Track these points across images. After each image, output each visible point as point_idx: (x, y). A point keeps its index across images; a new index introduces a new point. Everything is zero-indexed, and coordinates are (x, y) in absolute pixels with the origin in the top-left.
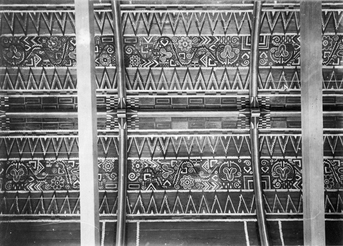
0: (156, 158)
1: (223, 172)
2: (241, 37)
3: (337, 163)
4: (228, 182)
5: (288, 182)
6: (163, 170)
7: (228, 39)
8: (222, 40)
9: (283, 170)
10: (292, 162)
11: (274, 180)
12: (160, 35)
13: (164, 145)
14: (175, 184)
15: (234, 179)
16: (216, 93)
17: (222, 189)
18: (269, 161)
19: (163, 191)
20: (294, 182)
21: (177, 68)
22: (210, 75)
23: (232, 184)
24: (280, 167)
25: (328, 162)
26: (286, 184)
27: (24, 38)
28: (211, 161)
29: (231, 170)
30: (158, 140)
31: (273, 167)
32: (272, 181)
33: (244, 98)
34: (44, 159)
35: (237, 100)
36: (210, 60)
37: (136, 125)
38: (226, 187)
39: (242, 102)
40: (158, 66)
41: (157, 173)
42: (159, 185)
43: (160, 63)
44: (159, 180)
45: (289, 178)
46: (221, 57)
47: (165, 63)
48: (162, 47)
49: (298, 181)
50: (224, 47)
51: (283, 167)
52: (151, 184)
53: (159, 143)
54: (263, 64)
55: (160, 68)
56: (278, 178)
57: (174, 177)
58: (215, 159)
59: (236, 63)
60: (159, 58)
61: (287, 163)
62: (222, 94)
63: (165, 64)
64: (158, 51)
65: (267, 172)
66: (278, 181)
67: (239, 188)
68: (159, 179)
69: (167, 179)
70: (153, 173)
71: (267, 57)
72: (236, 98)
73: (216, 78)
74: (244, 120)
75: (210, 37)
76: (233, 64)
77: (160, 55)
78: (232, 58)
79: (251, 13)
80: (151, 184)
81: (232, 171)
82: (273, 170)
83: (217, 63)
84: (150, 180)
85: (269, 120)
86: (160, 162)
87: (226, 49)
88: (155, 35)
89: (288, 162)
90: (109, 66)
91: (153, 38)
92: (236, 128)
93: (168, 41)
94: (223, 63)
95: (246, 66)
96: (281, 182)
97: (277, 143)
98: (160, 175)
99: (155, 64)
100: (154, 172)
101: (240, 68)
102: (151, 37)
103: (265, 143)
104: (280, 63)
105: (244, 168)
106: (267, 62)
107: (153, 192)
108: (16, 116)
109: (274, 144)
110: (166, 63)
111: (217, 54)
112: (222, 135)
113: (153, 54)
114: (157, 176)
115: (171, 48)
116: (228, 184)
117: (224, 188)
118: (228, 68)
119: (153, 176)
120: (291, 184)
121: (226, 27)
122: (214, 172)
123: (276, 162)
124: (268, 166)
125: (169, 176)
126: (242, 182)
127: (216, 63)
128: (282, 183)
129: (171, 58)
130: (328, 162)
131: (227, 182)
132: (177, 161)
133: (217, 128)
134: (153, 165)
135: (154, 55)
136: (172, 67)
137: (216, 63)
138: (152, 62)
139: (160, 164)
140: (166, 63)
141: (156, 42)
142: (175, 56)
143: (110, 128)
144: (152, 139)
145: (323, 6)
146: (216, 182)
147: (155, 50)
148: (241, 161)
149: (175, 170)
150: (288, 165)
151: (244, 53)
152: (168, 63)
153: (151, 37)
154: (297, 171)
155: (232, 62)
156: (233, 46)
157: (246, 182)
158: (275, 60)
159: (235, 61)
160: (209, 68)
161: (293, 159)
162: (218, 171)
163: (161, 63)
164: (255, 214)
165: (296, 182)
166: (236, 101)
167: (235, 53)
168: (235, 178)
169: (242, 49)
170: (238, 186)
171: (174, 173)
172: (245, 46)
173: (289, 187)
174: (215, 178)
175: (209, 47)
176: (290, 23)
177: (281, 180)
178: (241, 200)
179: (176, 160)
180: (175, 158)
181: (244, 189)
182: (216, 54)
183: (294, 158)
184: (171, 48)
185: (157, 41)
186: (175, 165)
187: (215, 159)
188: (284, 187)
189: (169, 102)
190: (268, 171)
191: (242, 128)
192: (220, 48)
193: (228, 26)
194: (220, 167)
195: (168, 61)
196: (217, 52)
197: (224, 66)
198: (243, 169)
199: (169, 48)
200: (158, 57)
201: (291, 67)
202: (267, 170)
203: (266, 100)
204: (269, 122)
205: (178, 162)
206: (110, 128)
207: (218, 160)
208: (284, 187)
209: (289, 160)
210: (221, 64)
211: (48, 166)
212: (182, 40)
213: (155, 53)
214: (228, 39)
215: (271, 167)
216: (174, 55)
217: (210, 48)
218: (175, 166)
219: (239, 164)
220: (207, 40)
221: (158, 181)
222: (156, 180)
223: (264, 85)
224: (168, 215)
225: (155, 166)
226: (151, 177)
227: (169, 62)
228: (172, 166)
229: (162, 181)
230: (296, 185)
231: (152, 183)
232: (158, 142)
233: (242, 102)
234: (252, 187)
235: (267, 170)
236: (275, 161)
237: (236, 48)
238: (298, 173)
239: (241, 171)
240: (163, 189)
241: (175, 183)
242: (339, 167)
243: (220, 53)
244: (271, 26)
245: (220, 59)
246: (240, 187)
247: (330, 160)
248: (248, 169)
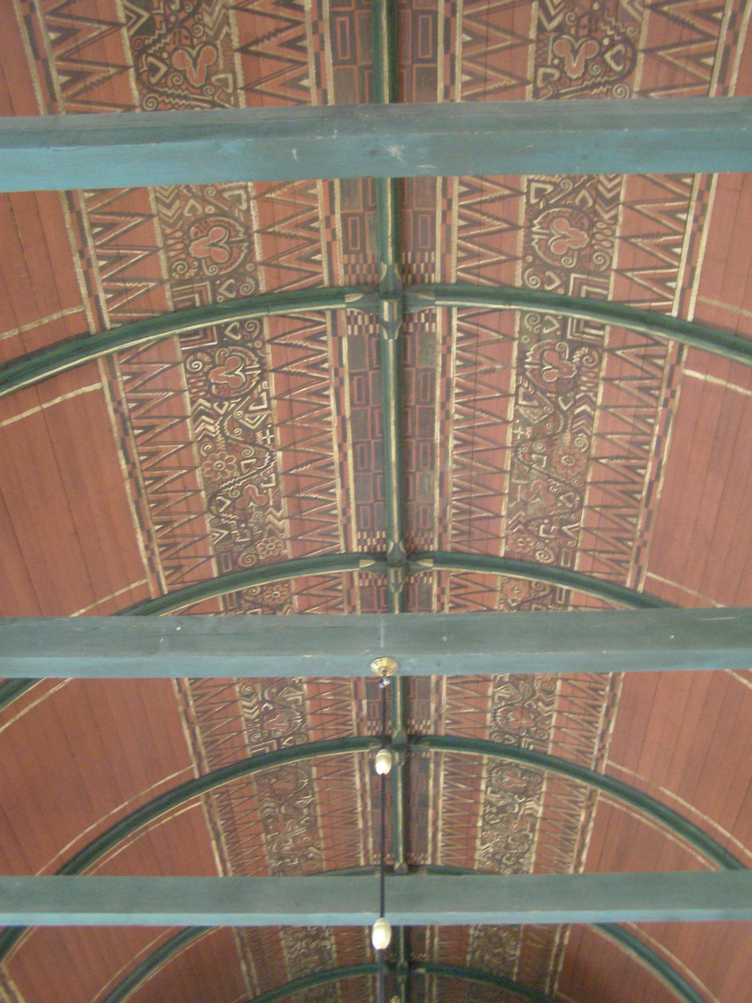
0: (232, 20)
1: (213, 227)
2: (608, 277)
7: (604, 243)
9: (237, 372)
10: (260, 390)
11: (208, 354)
12: (641, 45)
13: (281, 45)
14: (156, 96)
16: (449, 197)
17: (163, 230)
18: (257, 338)
19: (129, 59)
20: (208, 400)
21: (529, 88)
22: (502, 182)
23: (183, 256)
24: (245, 366)
25: (269, 465)
26: (201, 384)
28: (242, 192)
29: (221, 247)
30: (296, 23)
32: (202, 350)
33: (433, 270)
34: (238, 50)
36: (550, 188)
38: (171, 242)
39: (422, 265)
40: (541, 29)
41: (185, 32)
42: (147, 42)
43: (552, 35)
44: (163, 41)
45: (217, 388)
46: (554, 218)
47: (550, 52)
48: (603, 49)
49: (212, 408)
50: (582, 229)
51: (243, 371)
52: (146, 15)
53: (287, 28)
55: (532, 35)
56: (213, 362)
57: (179, 87)
59: (536, 256)
60: (569, 34)
61: (258, 378)
62: (444, 215)
63: (546, 52)
64: (589, 31)
65: (226, 336)
66: (204, 364)
67: (174, 274)
68: (168, 40)
69: (170, 67)
70: (182, 16)
71: (545, 331)
72: (433, 249)
74: (369, 271)
75: (617, 196)
76: (533, 248)
77: (577, 38)
78: (548, 248)
79: (670, 310)
80: (146, 15)
81: (220, 250)
82: (234, 350)
84: (159, 8)
86: (222, 37)
88: (645, 29)
89: (258, 382)
91: (634, 20)
92: (346, 251)
93: (618, 69)
94: (535, 222)
95: (523, 278)
96: (205, 370)
98: (180, 40)
99: (550, 19)
100: (186, 19)
102: (641, 14)
103: (308, 324)
104: (527, 360)
106: (530, 330)
107: (119, 26)
109: (306, 347)
110: (550, 57)
113: (582, 16)
114: (176, 30)
115: (596, 77)
116: (179, 246)
117: (166, 237)
118: (521, 234)
119: (173, 19)
120: (202, 394)
121: (639, 242)
122: (210, 203)
123: (256, 355)
124: (243, 337)
125: (180, 71)
126: (191, 281)
127: (538, 203)
128: (201, 374)
129: (563, 72)
130: (269, 465)
132: (230, 90)
134: (211, 14)
135: (579, 19)
137: (538, 203)
138: (555, 7)
139: (216, 36)
140: (550, 57)
141: (622, 30)
142: (570, 86)
144: (300, 44)
145: (710, 177)
147: (597, 22)
149: (201, 88)
150: (251, 383)
151: (560, 277)
152: (549, 63)
153: (641, 14)
154: (238, 404)
155: (536, 247)
156: (582, 253)
158: (534, 350)
159: (540, 254)
160: (526, 184)
161: (268, 391)
163: (551, 39)
164: (108, 325)
165: (208, 405)
167: (562, 256)
168: (199, 260)
169: (573, 276)
170: (177, 273)
171: (193, 86)
173: (194, 390)
174: (193, 209)
175: (587, 189)
176: (630, 393)
177: (209, 371)
179: (235, 88)
180: (241, 83)
181: (172, 287)
182: (565, 206)
184: (596, 77)
185: (624, 35)
186: (219, 87)
188: (192, 381)
189: (420, 56)
191: (346, 267)
193: (642, 249)
194: (226, 216)
195: (556, 62)
196: (570, 210)
198: (229, 278)
199: (595, 69)
200: (573, 31)
202: (234, 337)
204: (364, 331)
205: (230, 95)
208: (192, 381)
209: (265, 383)
213: (584, 21)
215: (243, 343)
216: (574, 83)
217: (584, 193)
218: (215, 86)
219: (243, 265)
220: (610, 186)
221: (161, 37)
222: (164, 31)
223: (469, 320)
224: (57, 88)
225: (207, 19)
226: (168, 12)
227: (553, 66)
228: (213, 79)
229: (163, 50)
230: (200, 405)
231: (149, 19)
232: (289, 24)
233: (422, 265)
234: (180, 306)
235: (234, 337)
236: (259, 352)
238: (233, 405)
240: (137, 58)
241: (162, 94)
242: (258, 486)
243: (566, 218)
244: (629, 350)
245: (550, 217)
247: (275, 467)
248: (229, 289)
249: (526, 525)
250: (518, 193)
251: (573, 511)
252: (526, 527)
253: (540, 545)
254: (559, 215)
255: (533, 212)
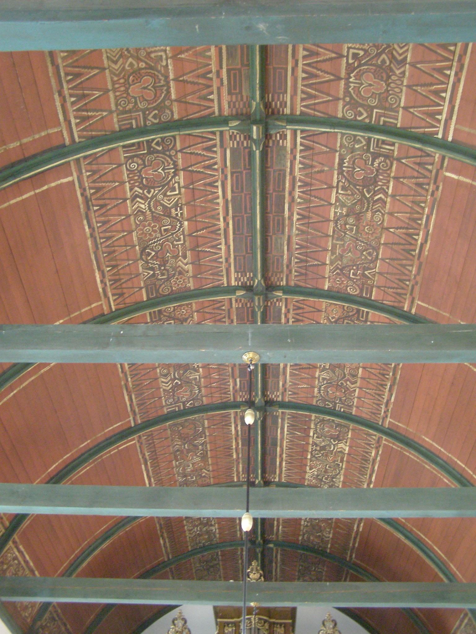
1: (144, 76)
2: (398, 112)
3: (179, 240)
4: (126, 88)
5: (140, 180)
6: (152, 89)
8: (396, 78)
9: (160, 170)
11: (141, 159)
15: (133, 97)
17: (112, 78)
18: (172, 149)
20: (141, 188)
23: (125, 95)
24: (164, 166)
25: (179, 230)
26: (136, 178)
27: (386, 194)
31: (163, 156)
33: (286, 106)
35: (281, 95)
37: (238, 143)
38: (117, 86)
39: (278, 102)
46: (363, 73)
54: (344, 140)
58: (167, 60)
59: (351, 98)
61: (172, 175)
66: (138, 165)
72: (286, 92)
73: (324, 61)
74: (244, 107)
76: (350, 92)
78: (360, 92)
81: (148, 91)
83: (353, 65)
85: (245, 145)
87: (378, 84)
90: (329, 282)
92: (230, 93)
94: (352, 75)
95: (343, 112)
97: (202, 108)
101: (341, 103)
105: (156, 112)
106: (347, 145)
108: (256, 57)
111: (371, 67)
112: (222, 228)
116: (122, 89)
117: (114, 83)
118: (343, 83)
120: (137, 184)
121: (419, 89)
122: (142, 61)
123: (172, 159)
124: (163, 148)
126: (130, 111)
128: (136, 172)
130: (179, 230)
131: (127, 85)
133: (228, 59)
136: (348, 52)
143: (232, 101)
146: (124, 68)
148: (168, 105)
155: (352, 92)
157: (175, 407)
159: (354, 96)
160: (346, 50)
161: (179, 183)
162: (145, 68)
164: (77, 140)
165: (141, 191)
166: (281, 93)
168: (135, 98)
169: (375, 110)
170: (121, 106)
172: (380, 116)
173: (132, 182)
176: (410, 187)
177: (141, 170)
178: (97, 114)
181: (118, 115)
182: (371, 65)
183: (182, 184)
187: (167, 60)
188: (131, 176)
190: (154, 148)
192: (382, 73)
194: (153, 70)
196: (374, 68)
197: (347, 77)
198: (154, 110)
201: (335, 180)
202: (158, 148)
203: (281, 141)
206: (232, 101)
207: (167, 65)
208: (131, 176)
209: (177, 177)
210: (352, 72)
211: (173, 210)
212: (375, 235)
214: (396, 90)
215: (163, 152)
217: (384, 56)
219: (163, 101)
220: (401, 52)
230: (136, 191)
233: (278, 102)
234: (123, 127)
236: (173, 157)
237: (379, 99)
238: (157, 192)
239: (149, 107)
244: (410, 160)
246: (121, 109)
247: (183, 231)
248: (155, 117)
249: (341, 270)
250: (341, 56)
251: (371, 262)
252: (342, 271)
253: (350, 283)
254: (367, 71)
255: (350, 69)
